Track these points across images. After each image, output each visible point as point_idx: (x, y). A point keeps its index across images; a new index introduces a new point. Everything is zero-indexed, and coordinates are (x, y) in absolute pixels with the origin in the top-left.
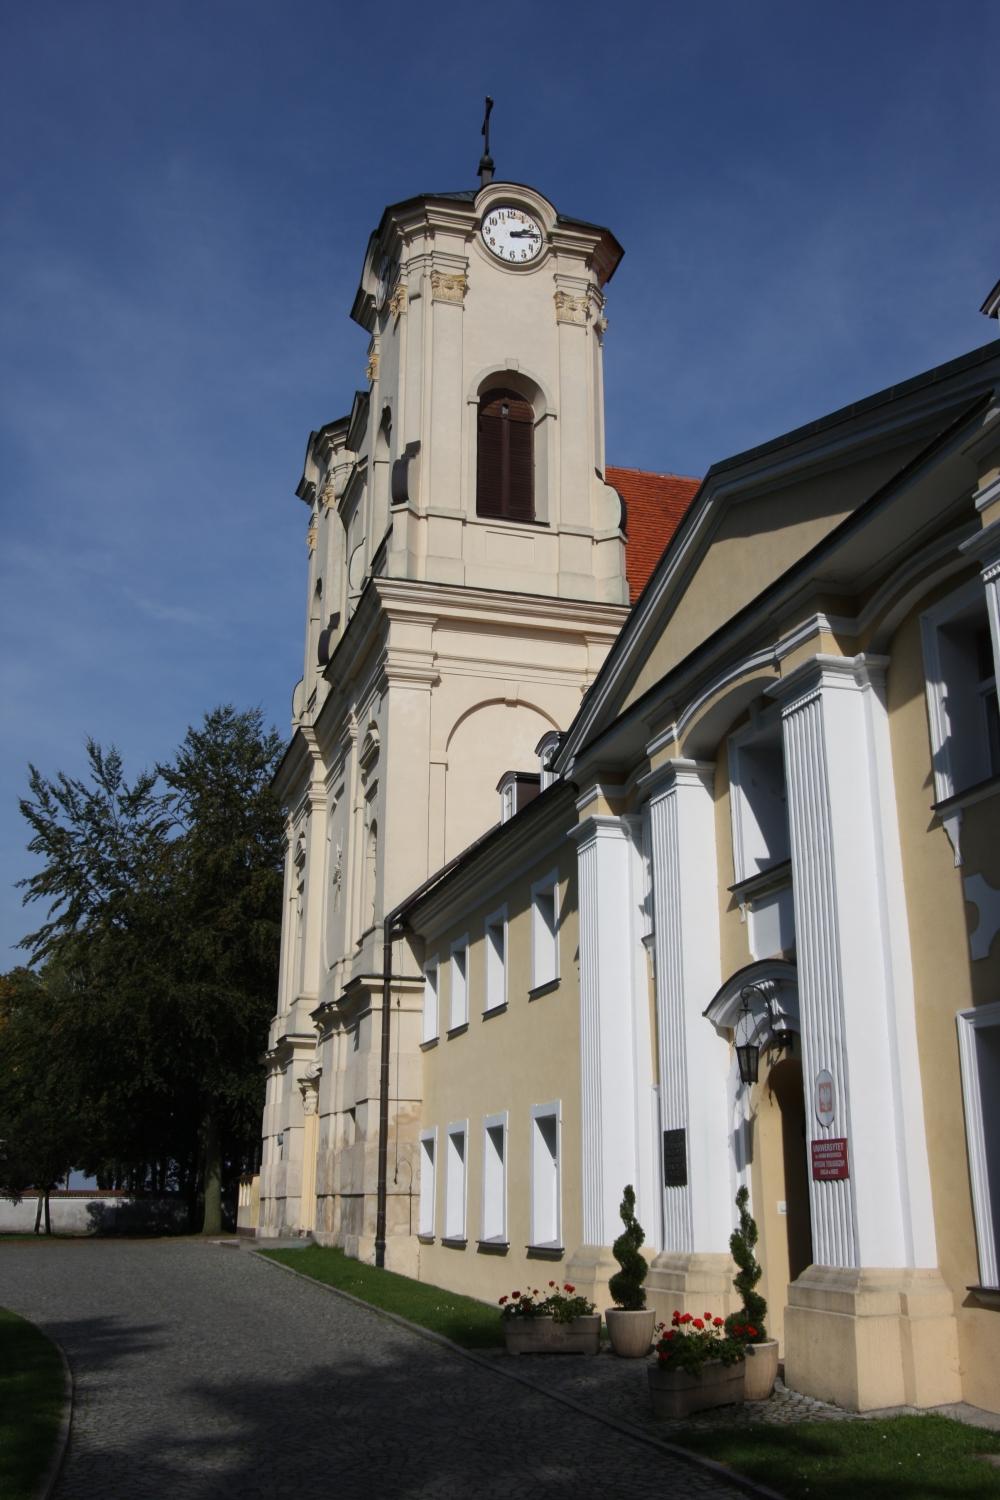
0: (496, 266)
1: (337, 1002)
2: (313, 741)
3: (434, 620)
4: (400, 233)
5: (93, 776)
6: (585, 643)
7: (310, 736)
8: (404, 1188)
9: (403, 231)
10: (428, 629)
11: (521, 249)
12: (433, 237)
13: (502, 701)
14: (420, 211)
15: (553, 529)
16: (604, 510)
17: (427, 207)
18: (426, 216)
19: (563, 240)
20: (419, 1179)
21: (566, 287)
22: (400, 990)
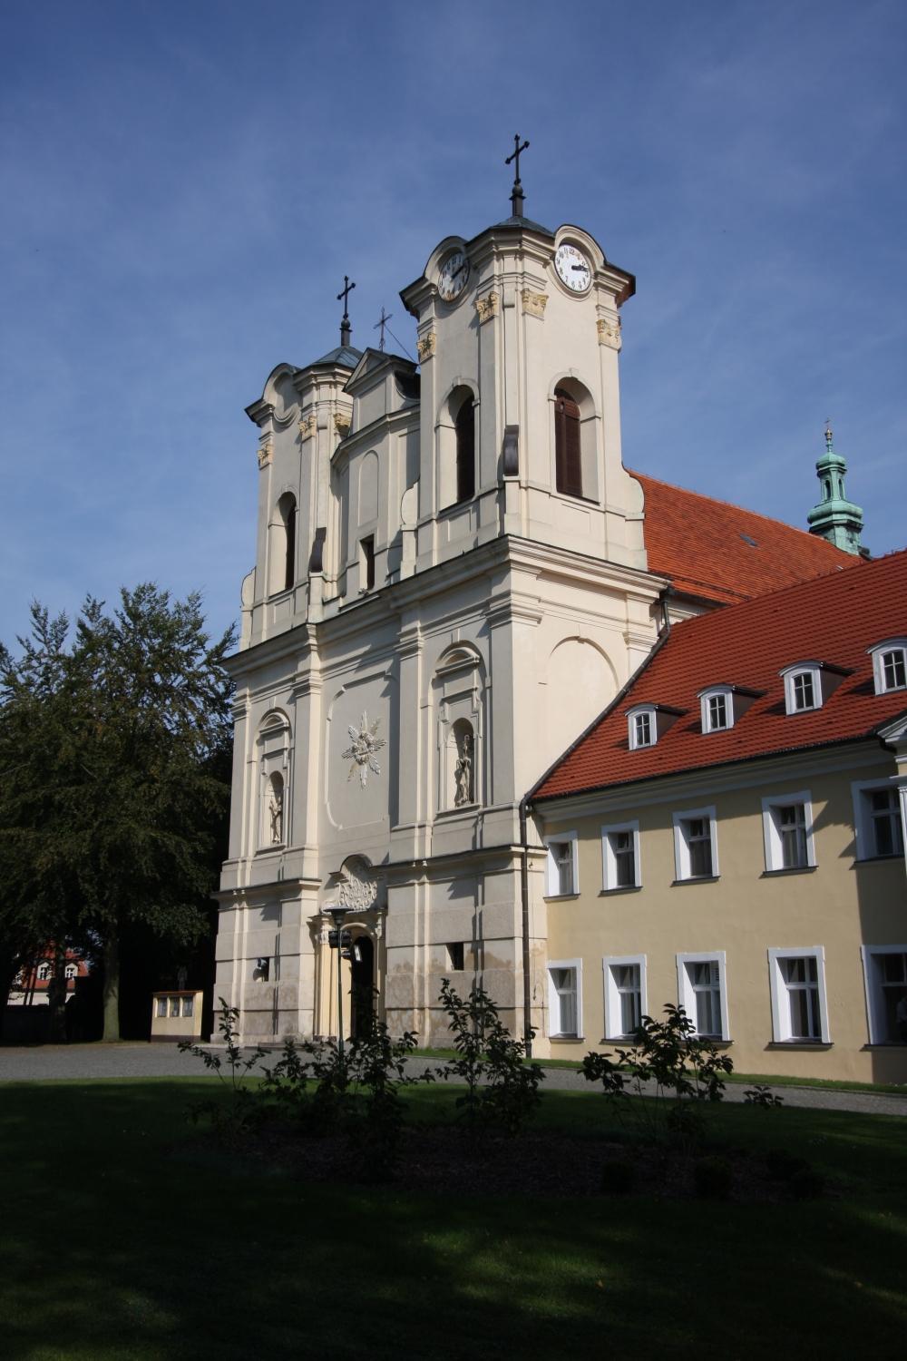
0: (561, 290)
1: (427, 860)
2: (313, 636)
3: (539, 572)
4: (495, 250)
5: (34, 635)
6: (625, 599)
7: (312, 632)
8: (539, 1004)
9: (497, 249)
10: (534, 577)
11: (578, 280)
12: (521, 259)
13: (576, 638)
14: (518, 237)
15: (601, 508)
16: (631, 499)
17: (524, 236)
18: (520, 242)
19: (605, 279)
20: (547, 996)
21: (605, 315)
22: (534, 856)
